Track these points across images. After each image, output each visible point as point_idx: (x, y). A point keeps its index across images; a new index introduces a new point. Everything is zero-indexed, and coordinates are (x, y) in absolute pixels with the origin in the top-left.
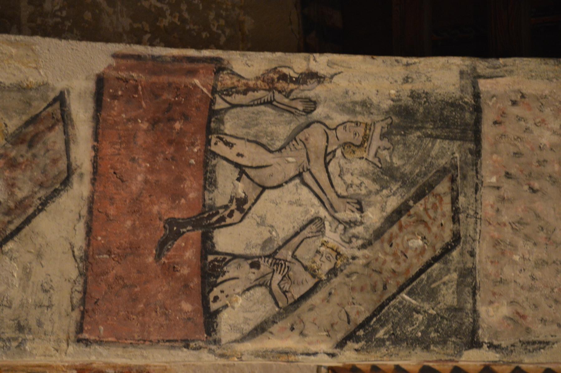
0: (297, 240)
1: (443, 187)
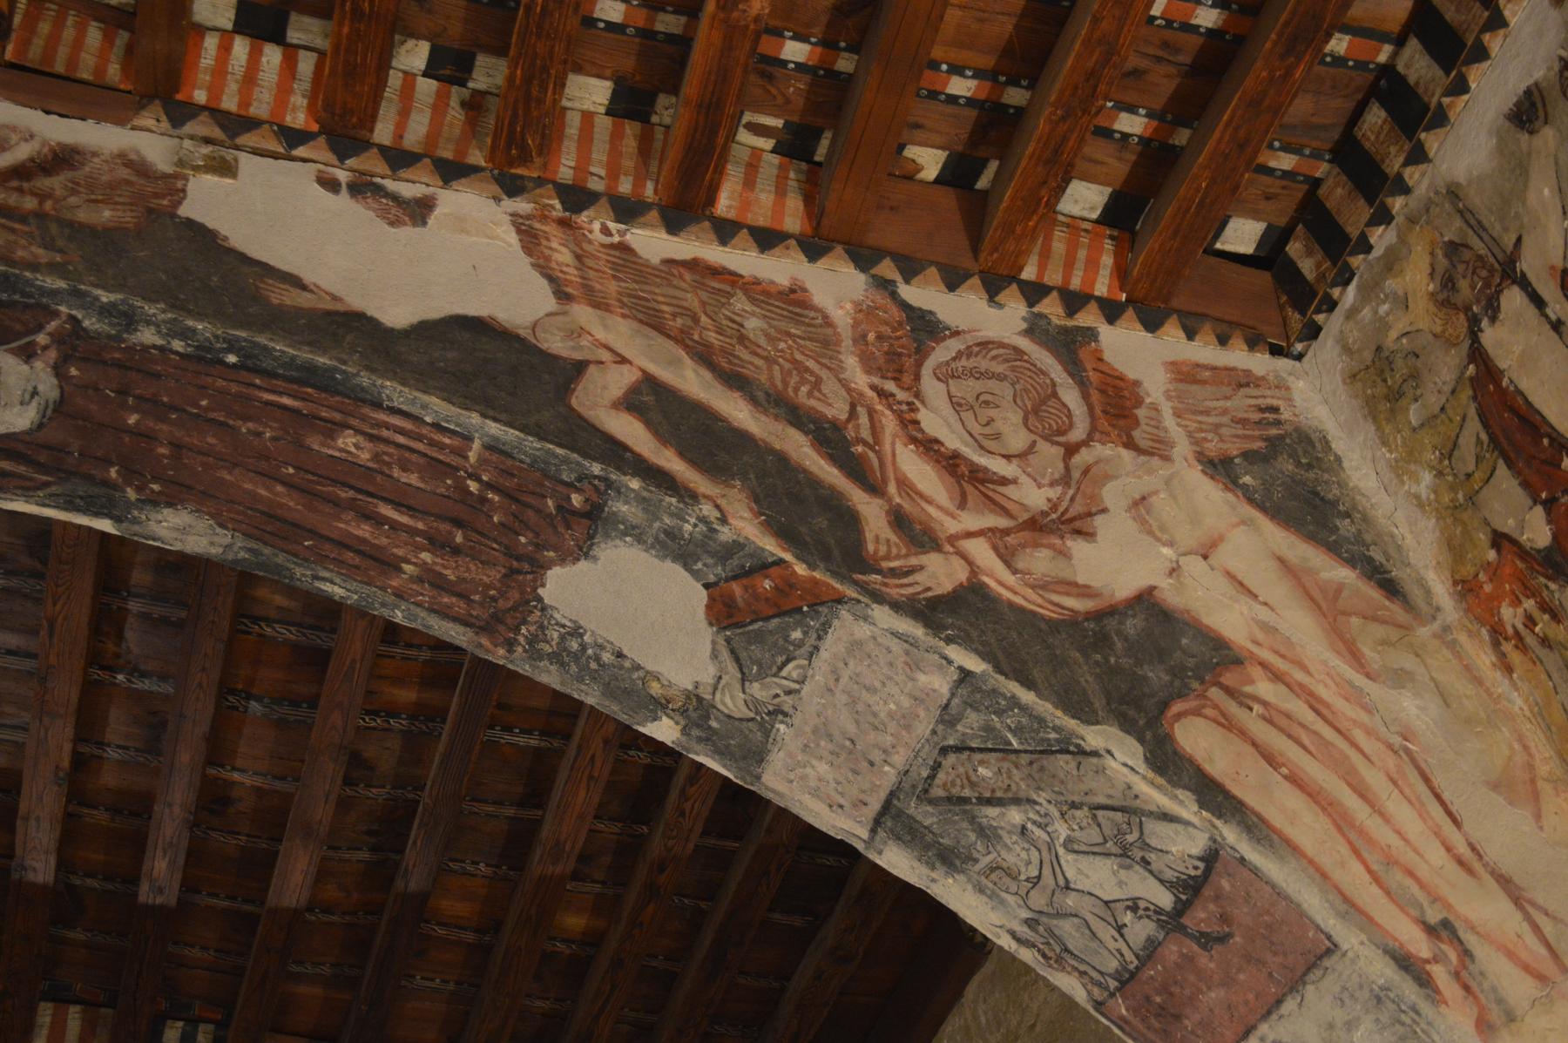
0: (1096, 849)
1: (937, 792)
